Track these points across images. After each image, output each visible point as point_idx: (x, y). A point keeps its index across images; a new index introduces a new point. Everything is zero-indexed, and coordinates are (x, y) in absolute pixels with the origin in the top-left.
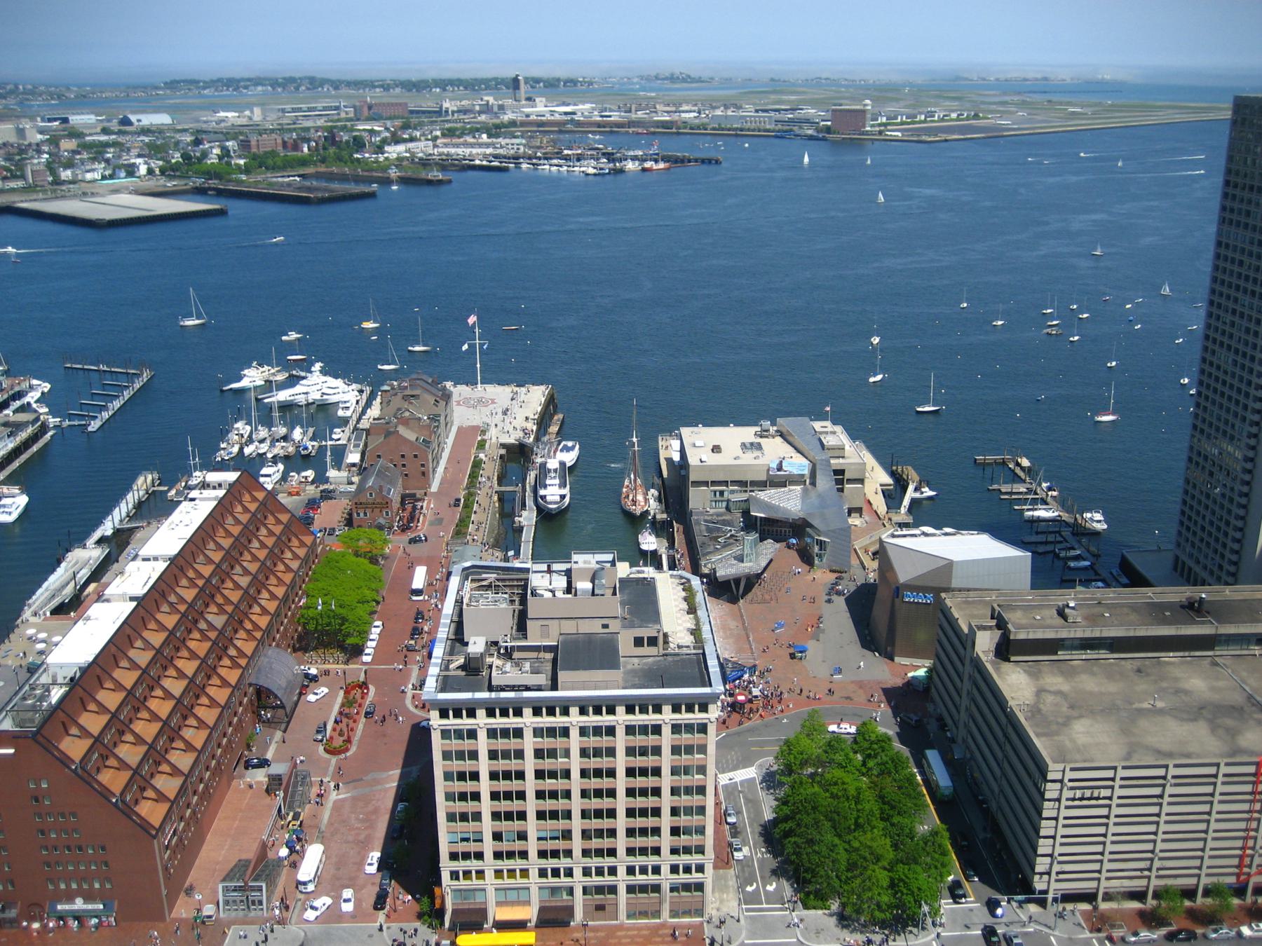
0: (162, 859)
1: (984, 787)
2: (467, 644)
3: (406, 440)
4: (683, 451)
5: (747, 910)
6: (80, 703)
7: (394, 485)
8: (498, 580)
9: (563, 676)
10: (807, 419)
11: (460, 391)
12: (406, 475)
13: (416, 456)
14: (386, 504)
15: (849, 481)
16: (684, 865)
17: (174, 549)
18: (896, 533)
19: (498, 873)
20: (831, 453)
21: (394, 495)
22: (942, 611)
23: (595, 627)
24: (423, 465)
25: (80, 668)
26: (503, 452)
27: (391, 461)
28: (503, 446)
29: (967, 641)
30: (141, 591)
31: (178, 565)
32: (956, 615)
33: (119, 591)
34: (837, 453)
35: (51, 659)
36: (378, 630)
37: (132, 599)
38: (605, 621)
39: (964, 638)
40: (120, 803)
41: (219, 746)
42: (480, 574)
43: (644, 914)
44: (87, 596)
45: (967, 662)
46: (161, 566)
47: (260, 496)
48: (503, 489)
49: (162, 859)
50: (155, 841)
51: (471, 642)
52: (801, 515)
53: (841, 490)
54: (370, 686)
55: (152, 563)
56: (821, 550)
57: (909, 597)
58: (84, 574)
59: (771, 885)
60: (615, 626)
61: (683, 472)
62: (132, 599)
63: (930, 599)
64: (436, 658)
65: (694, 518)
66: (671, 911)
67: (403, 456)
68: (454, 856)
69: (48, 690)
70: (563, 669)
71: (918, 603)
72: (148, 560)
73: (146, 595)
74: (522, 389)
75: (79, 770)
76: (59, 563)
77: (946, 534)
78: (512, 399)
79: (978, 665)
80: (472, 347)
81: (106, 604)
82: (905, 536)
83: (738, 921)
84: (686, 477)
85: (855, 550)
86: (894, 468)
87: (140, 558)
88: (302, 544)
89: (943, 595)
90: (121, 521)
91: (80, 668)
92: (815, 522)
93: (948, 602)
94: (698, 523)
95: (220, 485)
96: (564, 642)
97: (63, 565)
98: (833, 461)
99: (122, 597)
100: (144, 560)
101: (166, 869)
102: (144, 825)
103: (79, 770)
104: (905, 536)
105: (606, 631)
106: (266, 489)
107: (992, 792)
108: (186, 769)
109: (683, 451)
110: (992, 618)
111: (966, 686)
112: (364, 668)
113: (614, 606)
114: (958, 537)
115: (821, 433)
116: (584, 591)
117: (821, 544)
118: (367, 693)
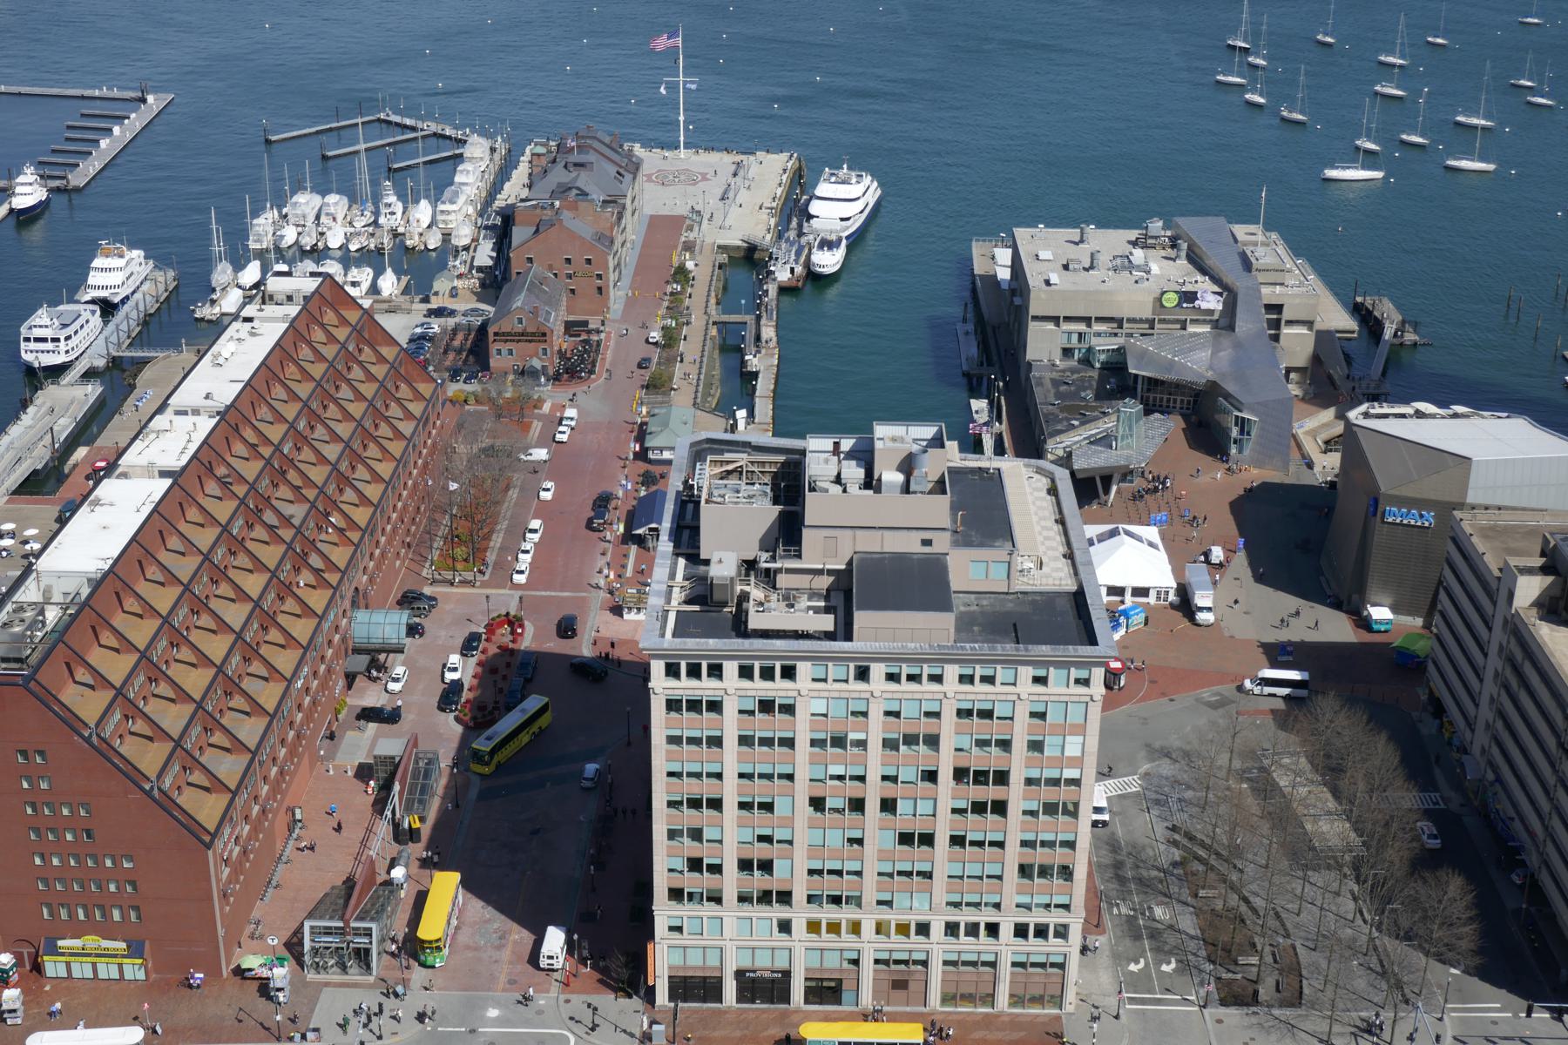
0: (218, 880)
1: (1517, 825)
2: (707, 562)
3: (573, 236)
4: (1017, 266)
5: (1132, 1001)
6: (90, 630)
7: (556, 307)
8: (752, 463)
9: (861, 618)
10: (1222, 220)
11: (651, 159)
12: (573, 291)
13: (589, 261)
14: (542, 336)
15: (1290, 323)
16: (1036, 925)
17: (227, 394)
18: (1372, 411)
19: (813, 927)
20: (1261, 278)
21: (556, 321)
22: (1454, 540)
23: (909, 544)
24: (599, 277)
25: (89, 580)
26: (724, 258)
27: (550, 268)
28: (722, 248)
29: (1498, 589)
30: (177, 461)
31: (231, 420)
32: (1481, 548)
33: (143, 460)
34: (1272, 277)
35: (43, 564)
36: (536, 537)
37: (164, 474)
38: (927, 535)
39: (1494, 585)
40: (156, 792)
41: (299, 707)
42: (721, 452)
43: (969, 998)
44: (75, 466)
45: (1498, 624)
46: (206, 424)
47: (353, 316)
48: (726, 318)
49: (218, 880)
50: (210, 853)
51: (714, 560)
52: (1210, 375)
53: (1276, 338)
54: (526, 623)
55: (190, 419)
56: (1242, 432)
57: (1394, 515)
58: (65, 426)
59: (1169, 963)
60: (942, 543)
61: (1017, 301)
62: (164, 474)
63: (1429, 519)
64: (659, 582)
65: (1034, 374)
66: (1011, 996)
67: (568, 261)
68: (676, 894)
69: (42, 612)
70: (861, 608)
71: (1409, 525)
72: (185, 413)
73: (184, 468)
74: (752, 158)
75: (95, 739)
76: (24, 405)
77: (1456, 416)
78: (735, 175)
79: (1517, 631)
80: (672, 87)
81: (123, 482)
82: (1385, 416)
83: (1117, 1017)
84: (1024, 308)
85: (1294, 437)
86: (1359, 299)
87: (170, 410)
88: (418, 396)
89: (1458, 514)
90: (119, 345)
91: (89, 580)
92: (1230, 387)
93: (1467, 527)
94: (1040, 384)
95: (290, 298)
96: (862, 560)
97: (31, 410)
98: (1265, 290)
99: (148, 471)
100: (178, 413)
101: (225, 895)
102: (191, 826)
103: (95, 739)
104: (1385, 416)
105: (927, 549)
106: (360, 307)
107: (1531, 834)
108: (252, 743)
109: (1017, 266)
110: (1543, 554)
111: (1494, 663)
112: (518, 593)
113: (938, 510)
114: (1476, 421)
115: (1245, 244)
116: (892, 485)
117: (1242, 424)
118: (521, 634)
